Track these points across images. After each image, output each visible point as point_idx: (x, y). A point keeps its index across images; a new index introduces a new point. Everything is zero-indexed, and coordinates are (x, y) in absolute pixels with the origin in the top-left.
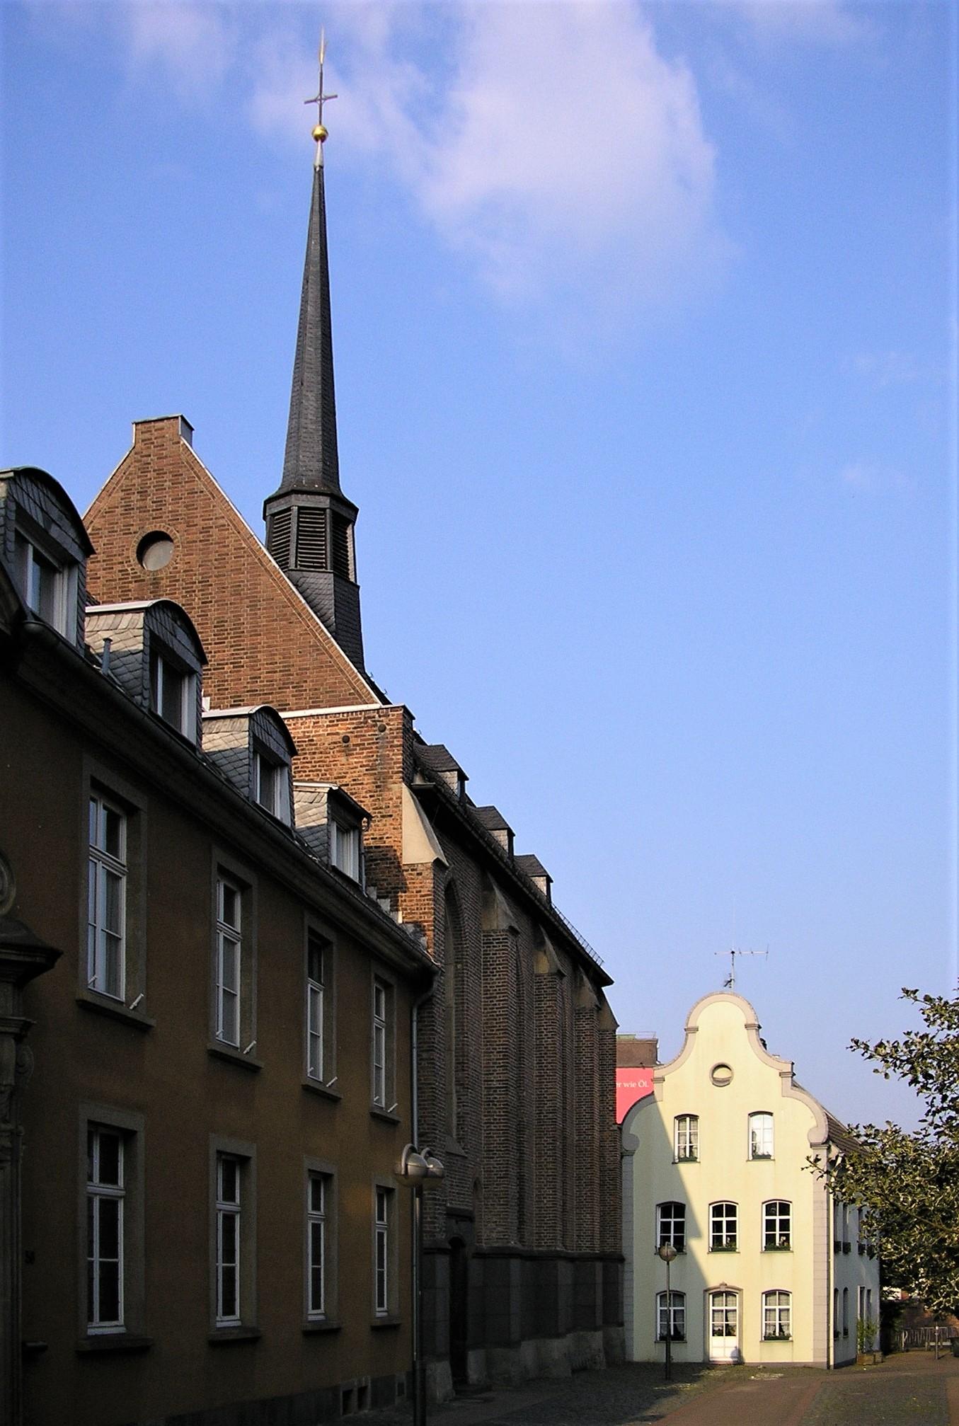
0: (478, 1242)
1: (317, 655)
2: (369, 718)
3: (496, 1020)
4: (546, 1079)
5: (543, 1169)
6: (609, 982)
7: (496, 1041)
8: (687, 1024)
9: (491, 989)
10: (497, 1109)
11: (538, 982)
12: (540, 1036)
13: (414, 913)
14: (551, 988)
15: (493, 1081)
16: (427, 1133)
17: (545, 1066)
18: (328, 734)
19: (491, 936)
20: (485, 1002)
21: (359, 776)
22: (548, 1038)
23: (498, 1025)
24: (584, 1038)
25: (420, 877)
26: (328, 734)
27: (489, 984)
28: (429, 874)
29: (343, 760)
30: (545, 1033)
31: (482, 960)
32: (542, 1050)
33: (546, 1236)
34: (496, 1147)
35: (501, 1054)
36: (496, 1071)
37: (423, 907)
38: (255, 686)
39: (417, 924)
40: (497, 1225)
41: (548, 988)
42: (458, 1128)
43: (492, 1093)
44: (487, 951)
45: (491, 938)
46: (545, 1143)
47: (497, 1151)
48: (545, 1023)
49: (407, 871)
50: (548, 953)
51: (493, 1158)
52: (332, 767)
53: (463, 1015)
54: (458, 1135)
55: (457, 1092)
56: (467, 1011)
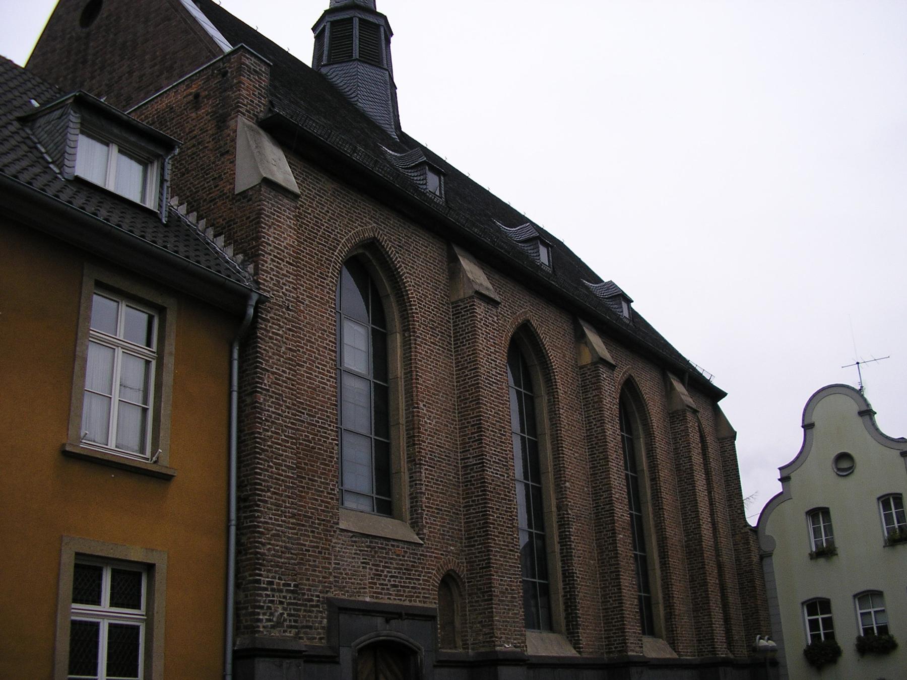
2: (215, 69)
3: (468, 391)
5: (605, 566)
6: (722, 395)
7: (470, 414)
9: (462, 360)
10: (475, 488)
11: (583, 374)
12: (590, 426)
14: (595, 377)
15: (469, 458)
19: (459, 306)
21: (205, 124)
22: (597, 427)
23: (471, 397)
26: (184, 97)
29: (193, 115)
30: (594, 423)
31: (452, 332)
32: (593, 441)
33: (616, 640)
34: (476, 533)
35: (476, 427)
37: (251, 233)
42: (411, 512)
43: (469, 471)
45: (460, 308)
47: (478, 537)
48: (593, 413)
51: (474, 545)
54: (412, 519)
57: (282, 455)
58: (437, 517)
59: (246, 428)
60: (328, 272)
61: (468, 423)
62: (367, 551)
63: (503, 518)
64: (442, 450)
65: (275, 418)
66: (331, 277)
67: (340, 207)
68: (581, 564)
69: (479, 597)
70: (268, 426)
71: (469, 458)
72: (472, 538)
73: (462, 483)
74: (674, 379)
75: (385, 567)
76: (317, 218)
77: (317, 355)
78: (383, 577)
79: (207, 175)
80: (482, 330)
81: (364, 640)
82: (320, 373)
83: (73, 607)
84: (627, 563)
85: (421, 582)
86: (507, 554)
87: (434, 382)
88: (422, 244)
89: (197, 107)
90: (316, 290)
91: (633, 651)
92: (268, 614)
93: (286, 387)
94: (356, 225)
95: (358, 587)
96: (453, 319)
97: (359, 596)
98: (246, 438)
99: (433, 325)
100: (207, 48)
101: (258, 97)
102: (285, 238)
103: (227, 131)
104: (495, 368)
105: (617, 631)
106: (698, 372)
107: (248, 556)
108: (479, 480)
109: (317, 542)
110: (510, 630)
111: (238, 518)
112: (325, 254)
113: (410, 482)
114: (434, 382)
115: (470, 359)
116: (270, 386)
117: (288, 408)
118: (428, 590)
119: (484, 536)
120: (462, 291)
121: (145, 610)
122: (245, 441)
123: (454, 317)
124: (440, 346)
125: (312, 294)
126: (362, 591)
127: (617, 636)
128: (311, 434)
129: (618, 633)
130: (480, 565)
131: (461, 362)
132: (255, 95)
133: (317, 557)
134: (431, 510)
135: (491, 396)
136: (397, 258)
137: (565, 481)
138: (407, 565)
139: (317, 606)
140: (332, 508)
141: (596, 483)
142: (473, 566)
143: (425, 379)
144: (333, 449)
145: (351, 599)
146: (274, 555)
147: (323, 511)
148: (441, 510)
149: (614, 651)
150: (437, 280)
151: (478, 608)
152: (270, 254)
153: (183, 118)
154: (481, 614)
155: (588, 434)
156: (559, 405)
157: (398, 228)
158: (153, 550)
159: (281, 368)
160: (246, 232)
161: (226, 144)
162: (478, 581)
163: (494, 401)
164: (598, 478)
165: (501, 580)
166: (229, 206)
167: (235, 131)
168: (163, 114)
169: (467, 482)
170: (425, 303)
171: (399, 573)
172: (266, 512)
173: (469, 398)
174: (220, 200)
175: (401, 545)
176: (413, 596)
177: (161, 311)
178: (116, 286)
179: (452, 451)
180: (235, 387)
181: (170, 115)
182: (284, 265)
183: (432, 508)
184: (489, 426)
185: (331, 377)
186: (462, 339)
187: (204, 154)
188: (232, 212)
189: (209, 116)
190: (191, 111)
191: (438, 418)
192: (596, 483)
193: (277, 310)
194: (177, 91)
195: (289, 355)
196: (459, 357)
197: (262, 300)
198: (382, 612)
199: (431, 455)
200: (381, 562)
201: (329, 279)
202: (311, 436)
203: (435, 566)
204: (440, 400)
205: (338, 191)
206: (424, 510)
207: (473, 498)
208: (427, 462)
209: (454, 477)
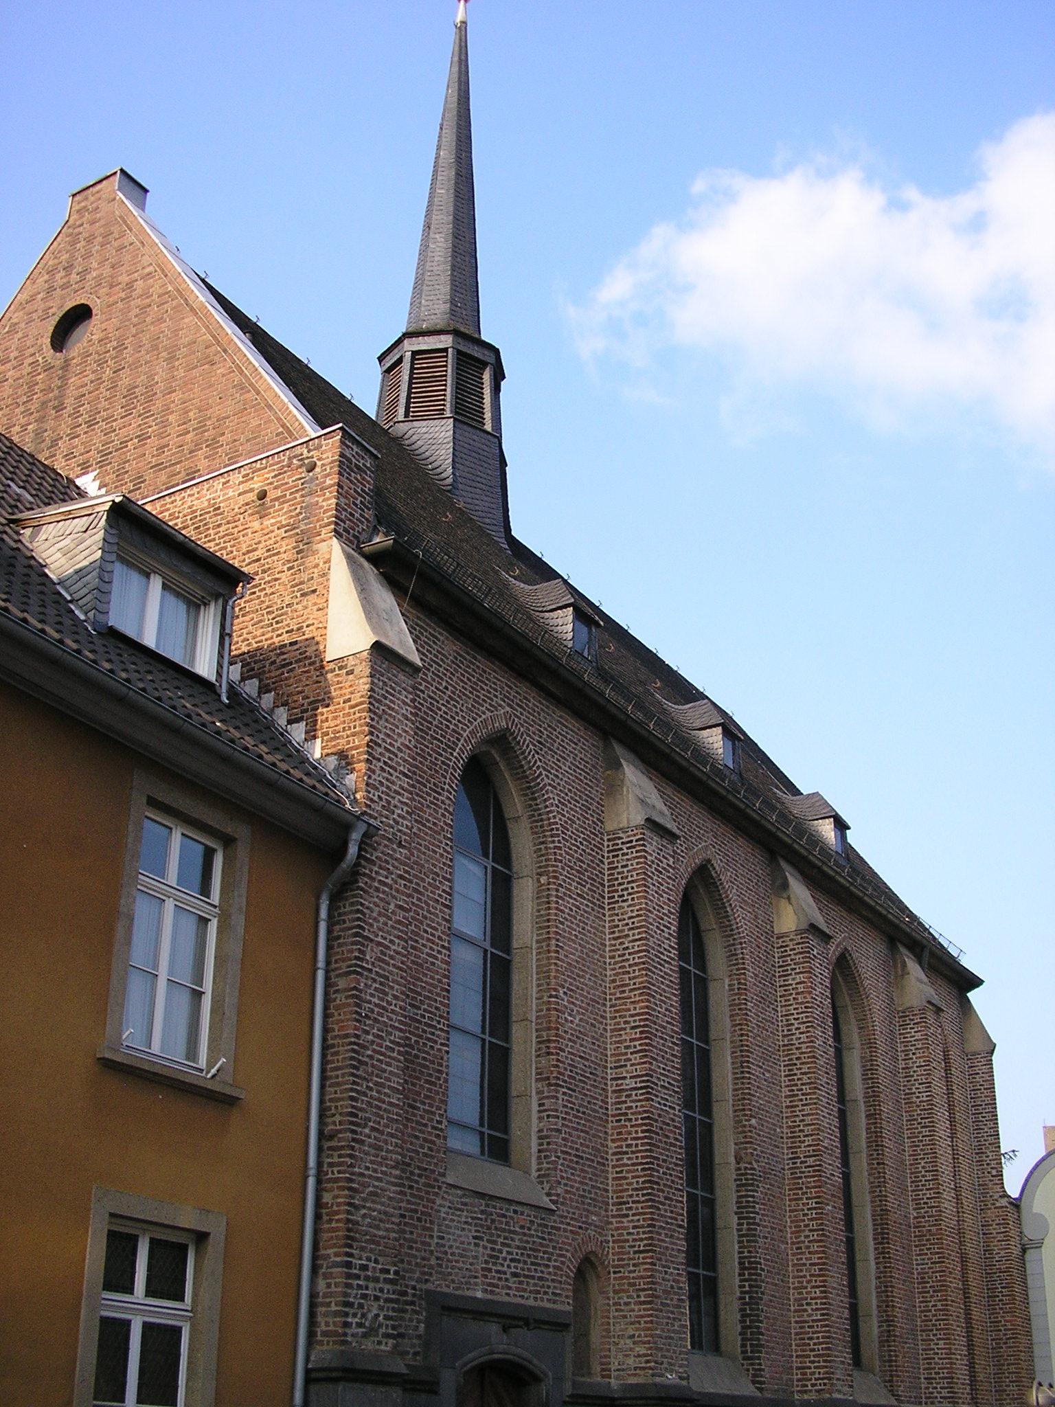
0: (603, 1377)
1: (241, 395)
4: (801, 1100)
6: (975, 982)
7: (629, 1010)
9: (620, 923)
11: (782, 947)
12: (789, 1030)
13: (338, 738)
15: (625, 1078)
16: (340, 1131)
18: (239, 495)
22: (801, 1033)
23: (632, 982)
24: (914, 1054)
28: (364, 669)
29: (256, 525)
34: (631, 1196)
35: (638, 1030)
37: (352, 725)
38: (162, 458)
39: (342, 755)
42: (539, 1158)
43: (624, 1099)
44: (613, 862)
45: (620, 842)
47: (634, 1202)
49: (333, 671)
50: (793, 900)
51: (627, 1216)
52: (242, 538)
53: (548, 958)
55: (538, 1093)
56: (557, 952)
57: (385, 1071)
59: (336, 1027)
60: (445, 784)
61: (626, 1022)
63: (671, 1175)
64: (586, 1063)
65: (379, 1013)
66: (448, 791)
67: (462, 681)
68: (767, 1249)
70: (369, 1025)
72: (625, 1203)
74: (908, 957)
75: (503, 1244)
76: (432, 698)
78: (500, 1261)
79: (277, 623)
80: (652, 879)
81: (474, 1357)
82: (428, 940)
83: (103, 1296)
84: (837, 1251)
85: (551, 1270)
86: (674, 1231)
87: (579, 957)
91: (839, 1391)
92: (359, 1316)
93: (394, 965)
94: (484, 709)
96: (608, 858)
97: (468, 1289)
98: (336, 1042)
99: (581, 867)
100: (279, 419)
101: (360, 509)
102: (399, 734)
104: (668, 939)
105: (817, 1359)
108: (640, 1113)
110: (675, 1352)
111: (319, 1164)
112: (441, 755)
113: (539, 1112)
115: (633, 923)
116: (373, 964)
117: (396, 997)
118: (560, 1282)
119: (643, 1202)
120: (625, 815)
121: (190, 1304)
122: (333, 1046)
125: (422, 817)
126: (472, 1281)
128: (415, 1035)
129: (819, 1362)
130: (634, 1246)
131: (618, 926)
132: (356, 505)
133: (416, 1227)
135: (662, 983)
136: (536, 762)
137: (751, 1116)
138: (534, 1242)
139: (413, 1303)
140: (438, 1151)
141: (795, 1122)
142: (622, 1247)
143: (567, 951)
145: (457, 1292)
146: (370, 1225)
147: (425, 1155)
148: (582, 1158)
149: (811, 1391)
150: (589, 797)
151: (628, 1314)
152: (379, 760)
153: (236, 526)
154: (632, 1323)
155: (786, 1043)
156: (746, 995)
159: (388, 937)
162: (630, 1272)
163: (665, 991)
164: (798, 1113)
167: (328, 561)
172: (361, 1158)
173: (628, 985)
177: (228, 842)
178: (174, 805)
179: (599, 1065)
180: (321, 963)
182: (397, 777)
184: (657, 1030)
185: (443, 947)
186: (622, 890)
187: (272, 590)
189: (283, 530)
191: (583, 1014)
192: (795, 1122)
193: (386, 846)
195: (400, 915)
198: (497, 1315)
199: (571, 1071)
200: (499, 1236)
201: (446, 793)
202: (414, 1039)
203: (570, 1245)
204: (586, 985)
205: (461, 656)
206: (558, 1157)
207: (629, 1142)
208: (565, 1081)
209: (601, 1107)
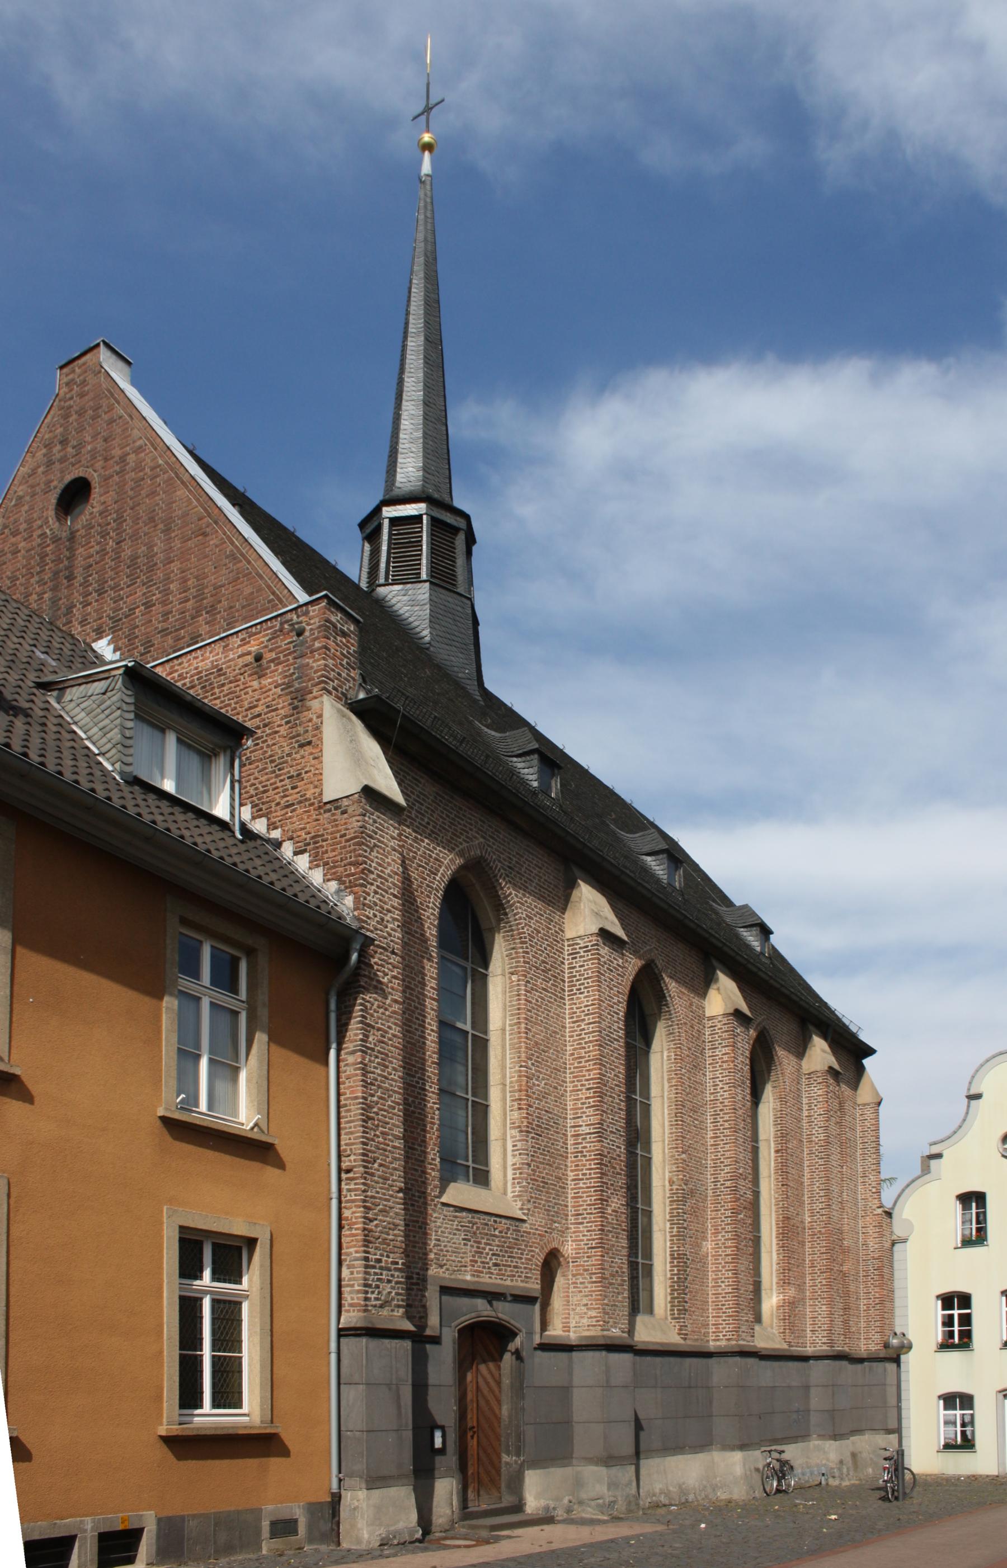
2: (287, 622)
3: (584, 1048)
5: (720, 1248)
6: (870, 1051)
8: (969, 1089)
10: (587, 1160)
17: (721, 1125)
19: (578, 944)
20: (570, 1027)
21: (273, 700)
22: (725, 1091)
24: (816, 1106)
25: (346, 816)
26: (239, 657)
27: (575, 1004)
29: (255, 684)
30: (721, 1086)
33: (724, 1328)
34: (586, 1210)
35: (592, 1091)
36: (584, 1113)
40: (588, 1309)
41: (722, 1032)
43: (580, 1141)
45: (577, 947)
46: (723, 1217)
47: (587, 1214)
48: (720, 1074)
52: (244, 696)
55: (512, 1137)
58: (542, 1191)
61: (582, 1085)
62: (468, 1227)
66: (432, 908)
69: (585, 1278)
71: (581, 1126)
72: (580, 1214)
73: (571, 1153)
75: (486, 1244)
77: (416, 1004)
79: (280, 770)
81: (466, 1319)
85: (523, 1261)
88: (536, 865)
89: (260, 673)
90: (416, 924)
93: (392, 1046)
94: (461, 840)
95: (459, 1264)
98: (348, 1102)
101: (347, 669)
103: (310, 715)
106: (844, 1024)
107: (354, 1232)
108: (593, 1151)
109: (417, 1216)
113: (513, 1151)
114: (544, 1036)
118: (531, 1269)
123: (570, 957)
124: (552, 993)
126: (463, 1269)
127: (727, 1324)
128: (411, 1096)
134: (536, 1183)
144: (434, 1114)
151: (583, 1290)
153: (238, 686)
157: (509, 844)
158: (255, 1224)
160: (341, 853)
161: (307, 731)
165: (612, 1262)
166: (314, 817)
167: (320, 716)
168: (206, 676)
169: (577, 1152)
170: (538, 940)
171: (501, 1251)
173: (584, 1057)
174: (301, 807)
175: (504, 1221)
176: (514, 1276)
181: (218, 679)
183: (537, 1181)
184: (607, 1090)
186: (580, 985)
188: (319, 825)
189: (279, 689)
190: (250, 678)
193: (381, 953)
194: (227, 645)
196: (574, 1006)
197: (369, 941)
199: (538, 1121)
201: (431, 910)
204: (550, 1058)
205: (440, 796)
208: (533, 1129)
